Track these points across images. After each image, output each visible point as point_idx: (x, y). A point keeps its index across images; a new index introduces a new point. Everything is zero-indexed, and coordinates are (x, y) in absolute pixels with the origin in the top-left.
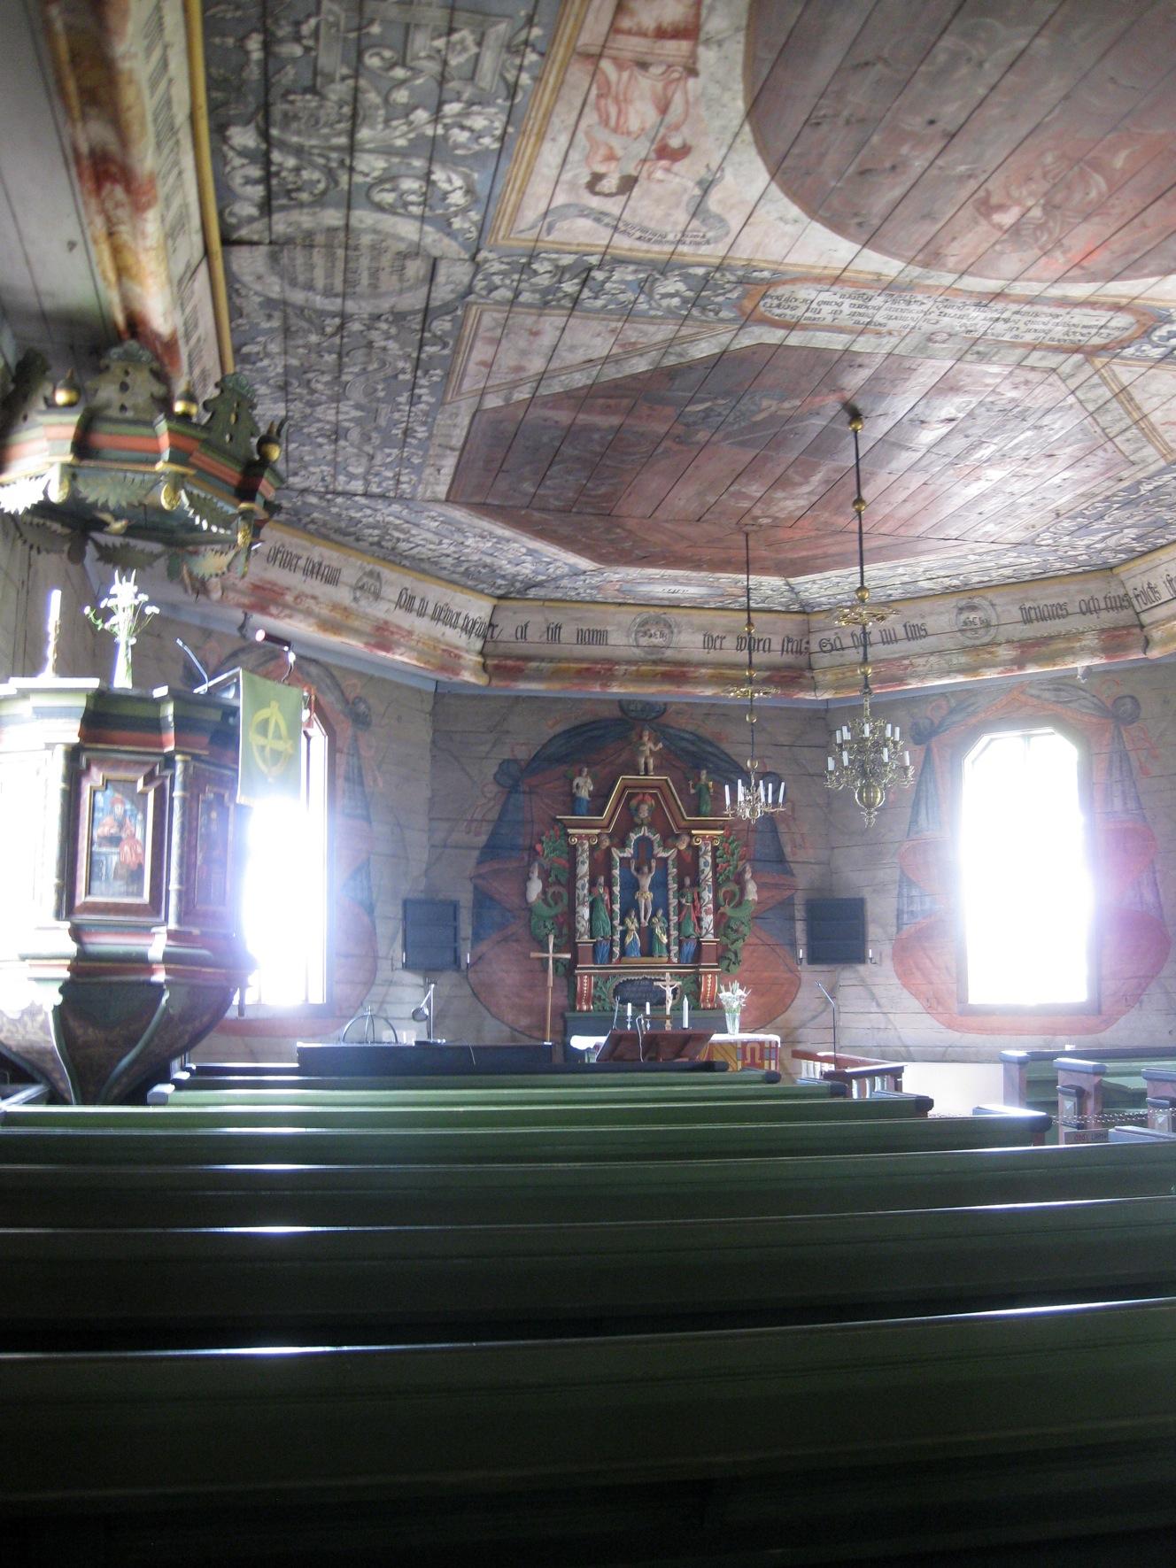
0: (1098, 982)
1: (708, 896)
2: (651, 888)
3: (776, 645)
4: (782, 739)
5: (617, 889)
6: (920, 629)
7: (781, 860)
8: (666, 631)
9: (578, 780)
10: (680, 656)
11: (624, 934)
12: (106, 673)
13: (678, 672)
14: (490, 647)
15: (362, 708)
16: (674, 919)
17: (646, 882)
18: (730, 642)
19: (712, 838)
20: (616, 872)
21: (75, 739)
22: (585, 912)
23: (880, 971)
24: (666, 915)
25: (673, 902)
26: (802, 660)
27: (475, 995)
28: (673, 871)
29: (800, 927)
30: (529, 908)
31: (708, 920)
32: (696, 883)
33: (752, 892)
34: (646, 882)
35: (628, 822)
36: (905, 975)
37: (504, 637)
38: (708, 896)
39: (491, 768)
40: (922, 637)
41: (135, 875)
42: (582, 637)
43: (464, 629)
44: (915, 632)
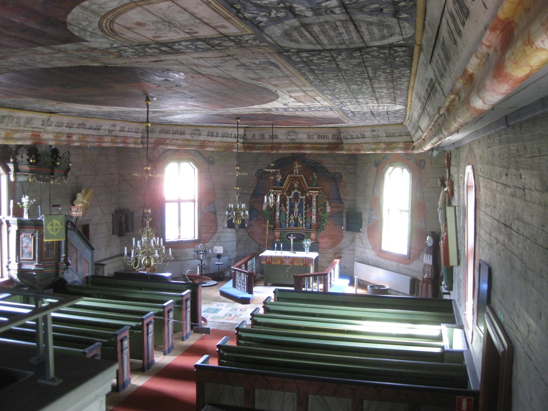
0: (410, 248)
1: (314, 210)
2: (298, 207)
3: (330, 137)
4: (342, 162)
5: (288, 207)
7: (339, 199)
9: (277, 176)
10: (301, 141)
11: (289, 220)
12: (22, 216)
13: (300, 145)
14: (245, 141)
16: (304, 216)
17: (296, 206)
18: (316, 137)
19: (315, 193)
20: (288, 202)
21: (17, 229)
22: (278, 214)
23: (364, 234)
24: (302, 215)
25: (304, 211)
26: (339, 141)
27: (249, 235)
28: (304, 202)
29: (344, 219)
30: (263, 211)
31: (314, 217)
32: (310, 206)
33: (328, 209)
34: (296, 206)
35: (292, 188)
36: (369, 237)
37: (249, 138)
38: (314, 210)
39: (255, 172)
41: (30, 254)
44: (363, 137)
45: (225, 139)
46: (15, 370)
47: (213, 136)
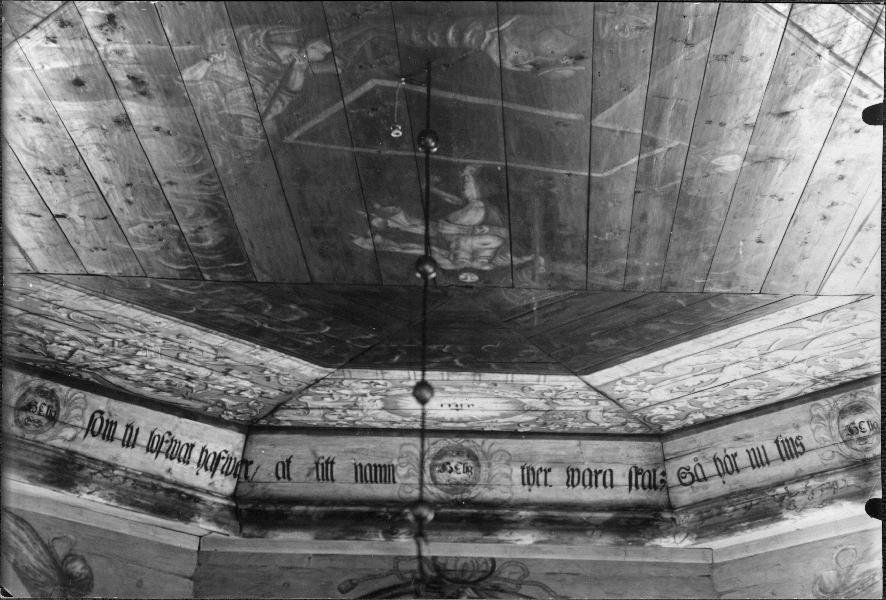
3: (621, 479)
6: (796, 444)
8: (470, 463)
13: (488, 518)
14: (245, 488)
15: (77, 567)
18: (557, 476)
40: (798, 454)
42: (362, 474)
43: (202, 464)
45: (159, 465)
46: (470, 99)
47: (110, 438)
